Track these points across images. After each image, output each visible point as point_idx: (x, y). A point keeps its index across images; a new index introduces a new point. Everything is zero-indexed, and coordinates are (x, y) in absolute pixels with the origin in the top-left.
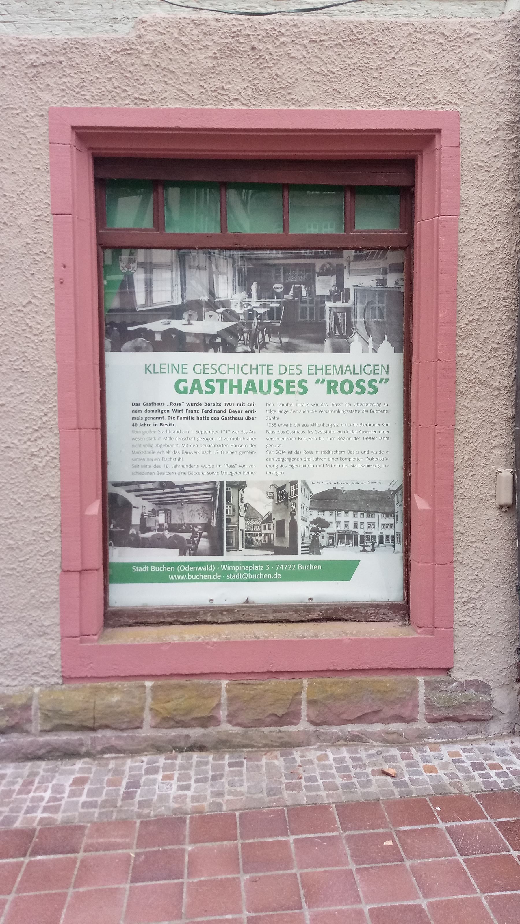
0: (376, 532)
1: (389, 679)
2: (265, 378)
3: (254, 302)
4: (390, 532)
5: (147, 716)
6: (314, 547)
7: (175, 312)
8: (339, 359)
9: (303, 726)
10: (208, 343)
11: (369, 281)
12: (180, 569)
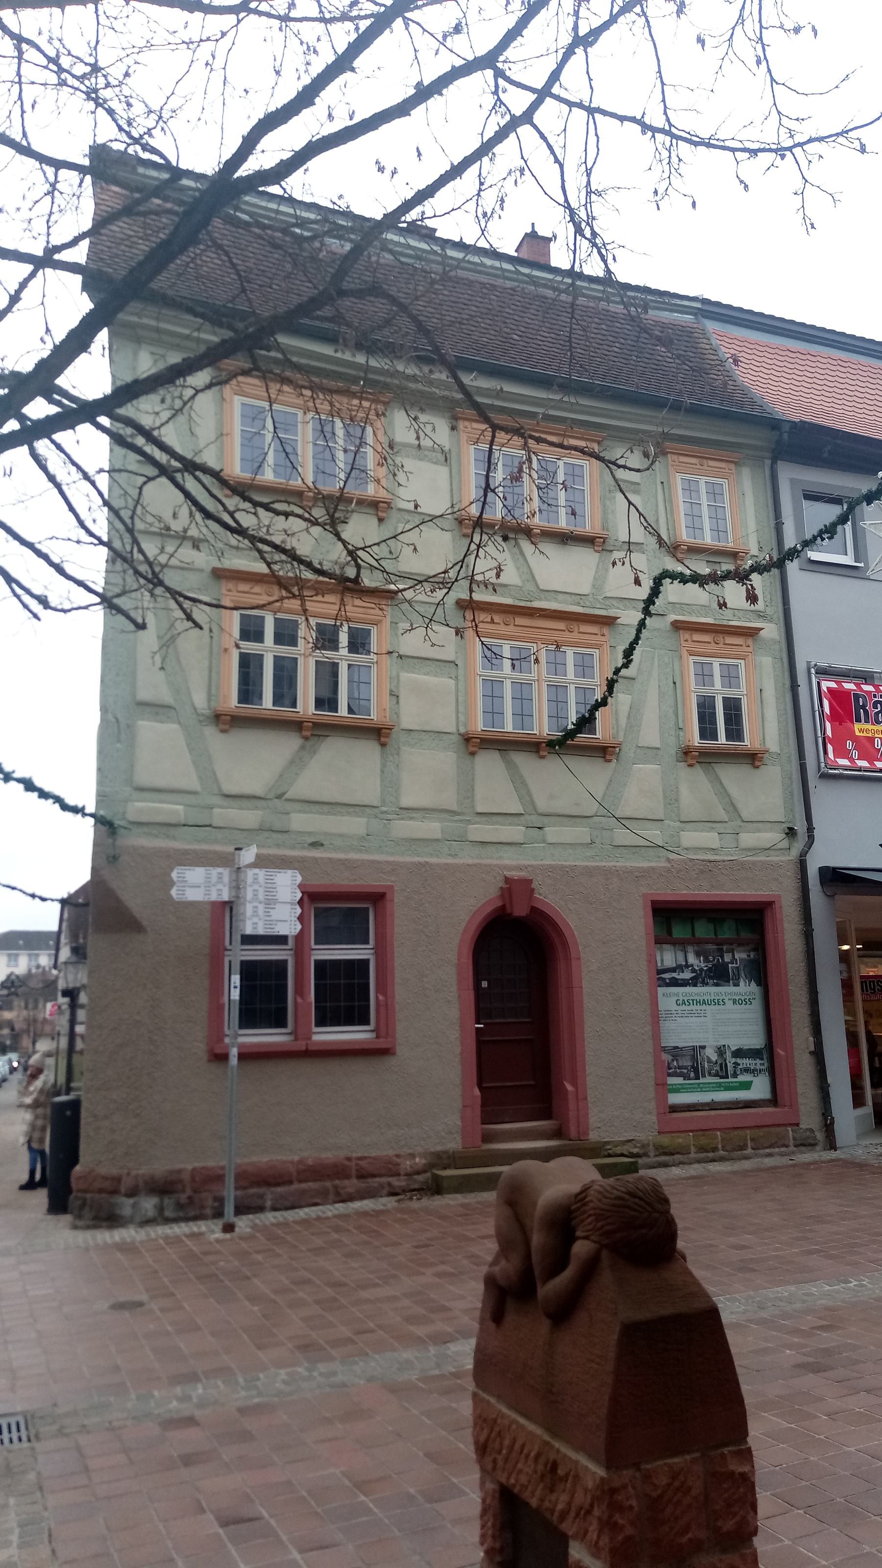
0: (758, 1067)
1: (778, 1129)
2: (709, 998)
3: (703, 965)
4: (763, 1067)
5: (693, 1149)
6: (735, 1075)
7: (673, 970)
8: (735, 989)
9: (749, 1151)
10: (684, 983)
11: (744, 956)
12: (685, 1086)
